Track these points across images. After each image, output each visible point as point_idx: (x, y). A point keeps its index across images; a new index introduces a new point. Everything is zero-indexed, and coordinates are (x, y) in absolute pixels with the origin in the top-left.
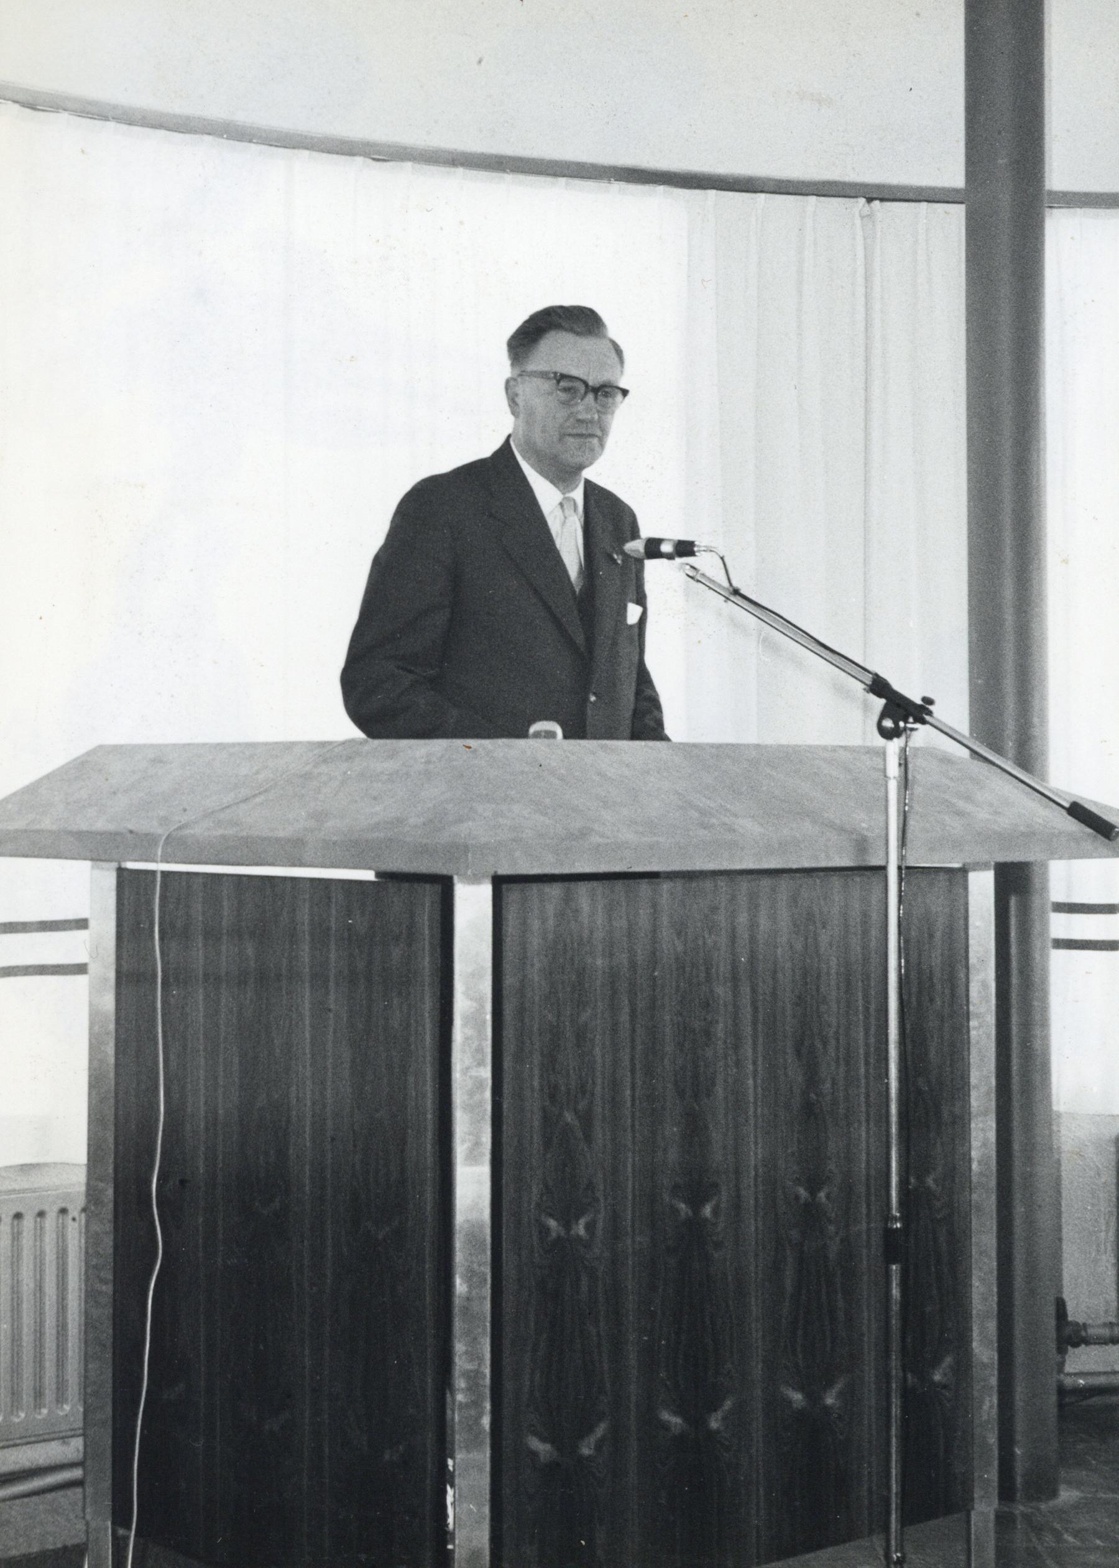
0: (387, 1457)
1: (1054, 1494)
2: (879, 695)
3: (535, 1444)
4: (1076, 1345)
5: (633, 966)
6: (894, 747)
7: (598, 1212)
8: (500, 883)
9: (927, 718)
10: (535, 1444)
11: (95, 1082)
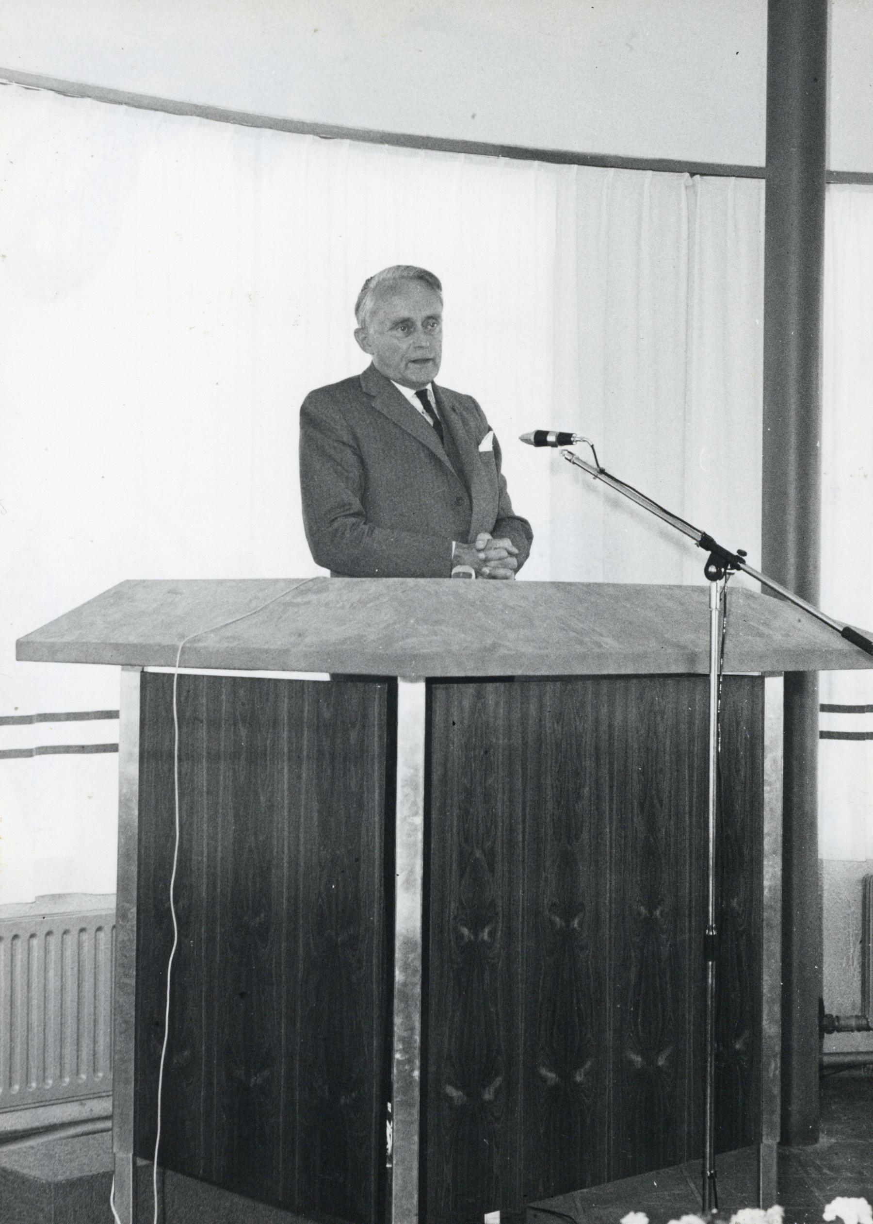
0: (342, 1101)
1: (816, 1140)
2: (707, 549)
3: (452, 1092)
4: (830, 1032)
5: (525, 744)
6: (716, 587)
7: (497, 922)
8: (431, 683)
9: (742, 565)
10: (452, 1092)
11: (123, 828)
